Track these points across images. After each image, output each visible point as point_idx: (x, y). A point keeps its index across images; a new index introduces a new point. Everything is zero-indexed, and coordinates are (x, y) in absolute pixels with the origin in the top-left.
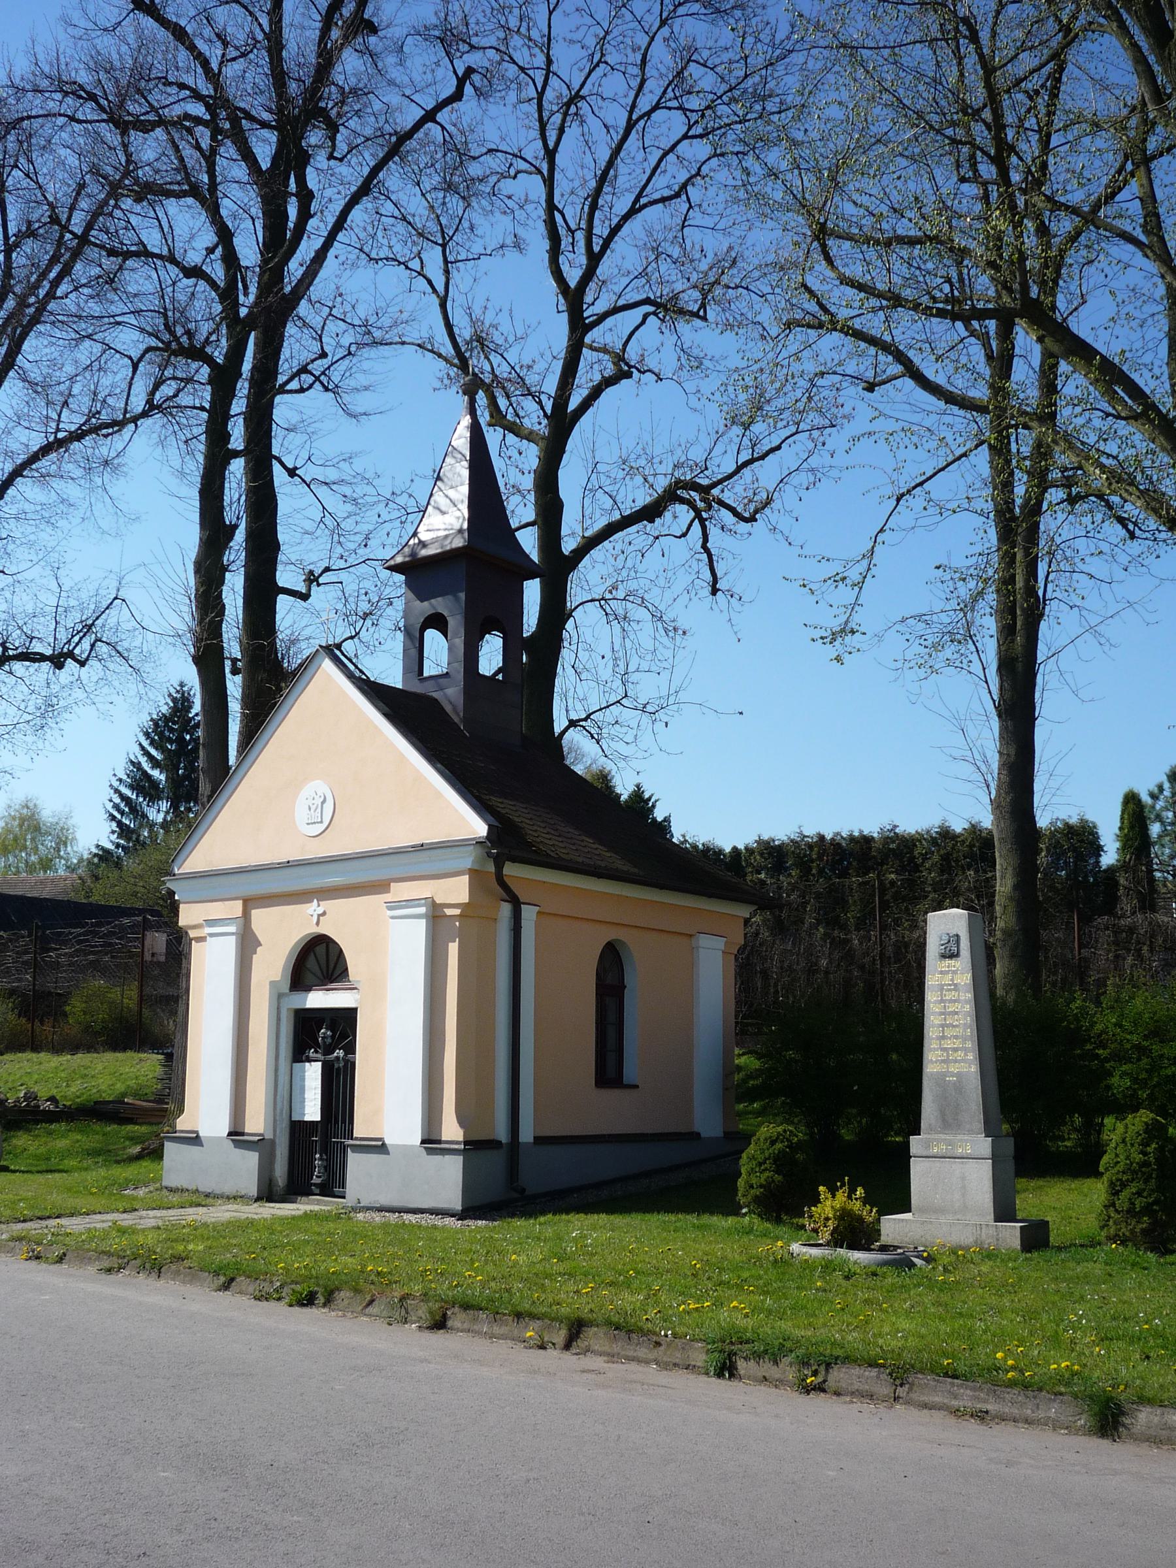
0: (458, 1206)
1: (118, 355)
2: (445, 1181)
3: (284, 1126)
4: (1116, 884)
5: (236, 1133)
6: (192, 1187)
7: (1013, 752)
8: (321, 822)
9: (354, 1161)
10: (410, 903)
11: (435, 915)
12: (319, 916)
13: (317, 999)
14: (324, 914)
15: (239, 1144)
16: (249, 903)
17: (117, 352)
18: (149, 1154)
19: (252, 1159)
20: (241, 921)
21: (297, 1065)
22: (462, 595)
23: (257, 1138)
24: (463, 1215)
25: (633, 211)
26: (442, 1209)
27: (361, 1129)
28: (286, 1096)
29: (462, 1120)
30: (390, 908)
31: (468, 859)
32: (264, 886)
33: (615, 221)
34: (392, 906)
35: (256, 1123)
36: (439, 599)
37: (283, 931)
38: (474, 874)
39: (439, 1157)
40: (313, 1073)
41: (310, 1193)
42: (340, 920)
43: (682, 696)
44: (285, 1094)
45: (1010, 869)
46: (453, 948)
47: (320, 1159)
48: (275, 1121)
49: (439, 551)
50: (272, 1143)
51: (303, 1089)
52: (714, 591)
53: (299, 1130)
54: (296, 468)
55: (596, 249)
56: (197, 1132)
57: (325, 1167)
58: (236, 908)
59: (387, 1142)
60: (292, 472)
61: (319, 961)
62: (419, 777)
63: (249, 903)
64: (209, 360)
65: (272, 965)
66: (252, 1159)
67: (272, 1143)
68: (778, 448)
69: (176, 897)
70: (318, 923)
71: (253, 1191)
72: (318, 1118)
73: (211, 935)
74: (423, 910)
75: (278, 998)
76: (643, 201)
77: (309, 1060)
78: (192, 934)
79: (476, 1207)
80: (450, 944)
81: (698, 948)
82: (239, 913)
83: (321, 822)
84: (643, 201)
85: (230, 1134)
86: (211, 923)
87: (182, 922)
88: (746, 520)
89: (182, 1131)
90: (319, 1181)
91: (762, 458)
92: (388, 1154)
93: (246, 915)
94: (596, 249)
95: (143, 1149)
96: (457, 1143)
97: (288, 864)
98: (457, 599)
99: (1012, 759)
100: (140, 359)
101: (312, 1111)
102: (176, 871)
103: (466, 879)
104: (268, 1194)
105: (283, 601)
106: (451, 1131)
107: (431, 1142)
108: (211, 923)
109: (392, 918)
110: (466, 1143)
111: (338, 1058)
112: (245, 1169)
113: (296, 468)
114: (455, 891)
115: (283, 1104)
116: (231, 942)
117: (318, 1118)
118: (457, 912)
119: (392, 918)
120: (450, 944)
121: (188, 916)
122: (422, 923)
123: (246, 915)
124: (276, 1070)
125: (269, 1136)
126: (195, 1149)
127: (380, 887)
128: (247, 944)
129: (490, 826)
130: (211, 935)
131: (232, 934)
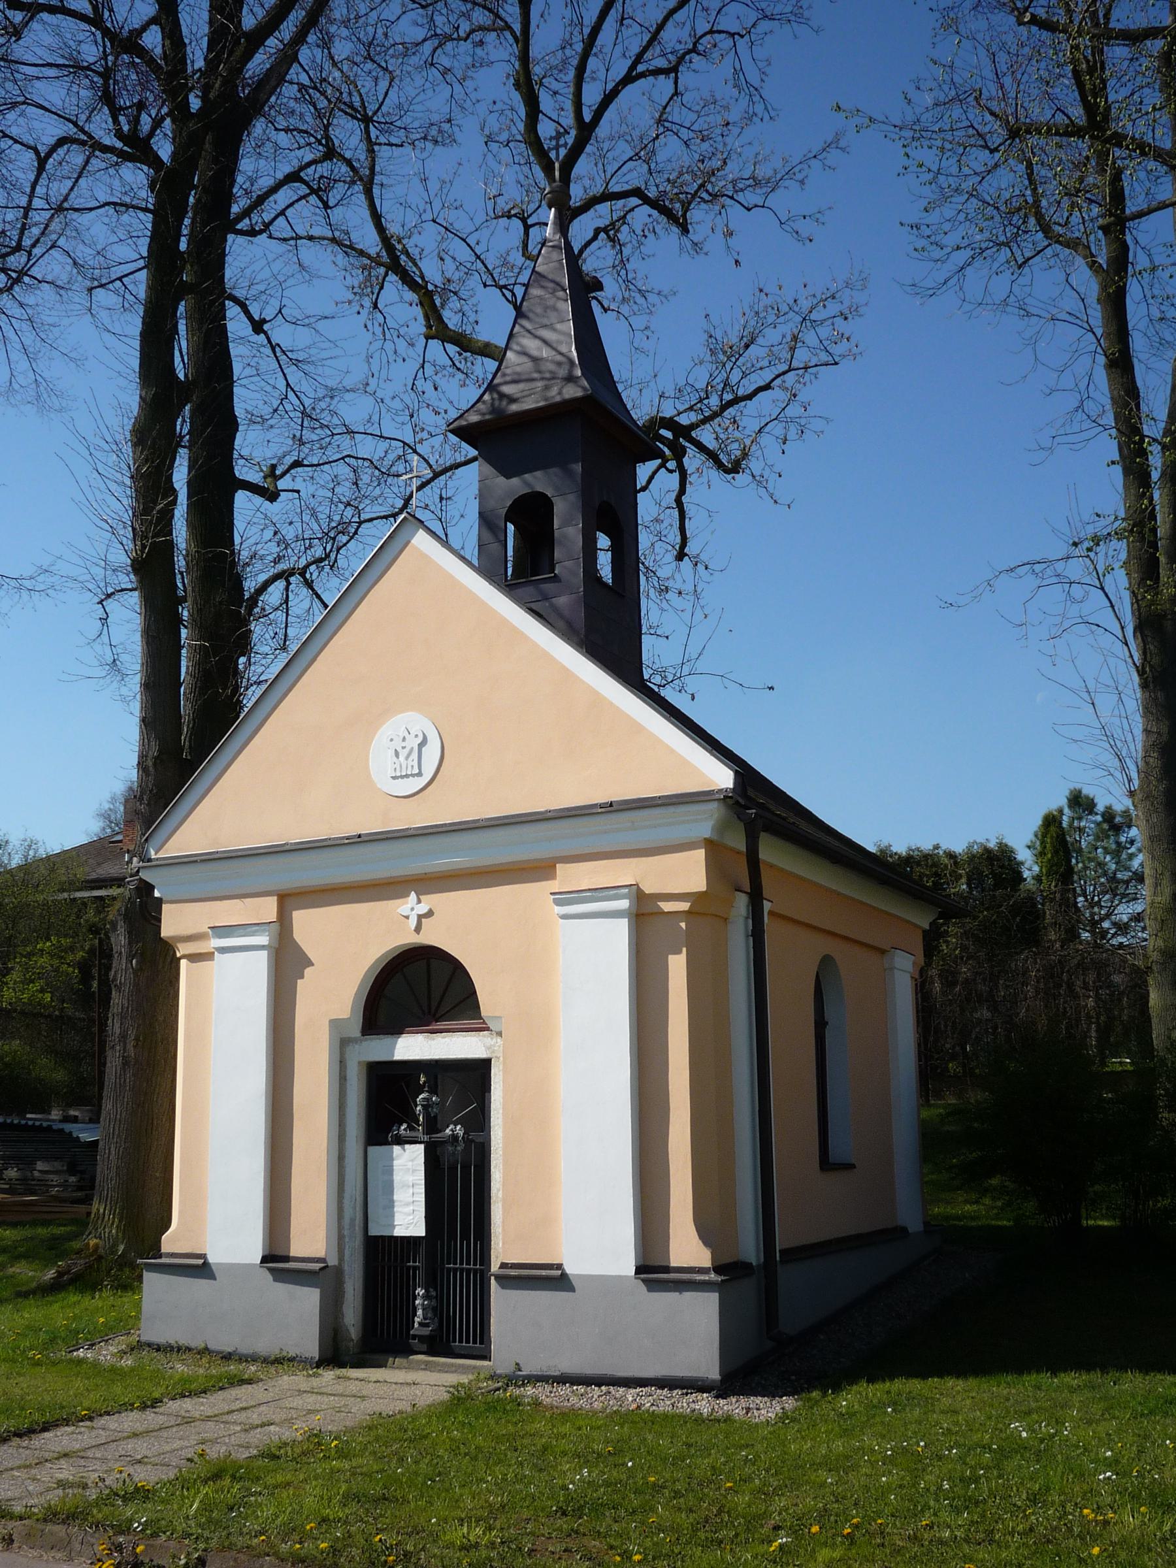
0: (713, 1373)
1: (17, 147)
2: (691, 1334)
3: (355, 1246)
4: (1039, 916)
5: (275, 1258)
6: (197, 1343)
7: (1165, 729)
8: (420, 774)
9: (503, 1304)
10: (598, 893)
11: (644, 912)
12: (420, 917)
13: (413, 1047)
14: (430, 914)
15: (281, 1276)
16: (288, 901)
17: (16, 141)
18: (72, 1281)
19: (309, 1299)
20: (276, 927)
21: (373, 1150)
22: (578, 468)
23: (317, 1266)
24: (725, 1388)
25: (629, 79)
26: (697, 1380)
27: (507, 1244)
28: (360, 1199)
29: (706, 1232)
30: (558, 903)
31: (705, 821)
32: (305, 877)
33: (610, 86)
34: (562, 898)
35: (311, 1238)
36: (538, 474)
37: (348, 945)
38: (712, 847)
39: (674, 1296)
40: (408, 1165)
41: (407, 1351)
42: (453, 923)
43: (700, 666)
44: (360, 1195)
45: (1168, 874)
46: (677, 965)
47: (425, 1297)
48: (341, 1237)
49: (542, 404)
50: (338, 1272)
51: (389, 1188)
52: (681, 556)
53: (384, 1255)
54: (264, 321)
55: (587, 117)
56: (203, 1256)
57: (434, 1309)
58: (268, 908)
59: (569, 1270)
60: (258, 326)
61: (421, 986)
62: (597, 700)
63: (288, 901)
64: (153, 161)
65: (333, 992)
66: (309, 1299)
67: (338, 1272)
68: (767, 387)
69: (157, 894)
70: (418, 929)
71: (312, 1348)
72: (420, 1231)
73: (223, 950)
74: (624, 904)
75: (342, 1044)
76: (641, 68)
77: (401, 1141)
78: (182, 950)
79: (737, 1378)
80: (672, 959)
81: (892, 969)
82: (272, 915)
83: (420, 774)
84: (641, 68)
85: (265, 1260)
86: (221, 931)
87: (166, 931)
88: (727, 471)
89: (173, 1255)
90: (426, 1331)
91: (749, 397)
92: (215, 1279)
93: (284, 921)
94: (587, 117)
95: (60, 1274)
96: (701, 1271)
97: (359, 840)
98: (570, 474)
99: (1165, 738)
100: (49, 154)
101: (408, 1217)
102: (153, 855)
103: (700, 854)
104: (335, 1354)
105: (241, 497)
106: (687, 1249)
107: (653, 1270)
108: (221, 931)
109: (565, 917)
110: (717, 1269)
111: (455, 1137)
112: (297, 1317)
113: (264, 321)
114: (684, 874)
115: (352, 1210)
116: (261, 961)
117: (420, 1231)
118: (684, 906)
119: (565, 917)
120: (672, 959)
121: (174, 922)
122: (623, 925)
123: (284, 921)
124: (341, 1158)
125: (333, 1261)
126: (202, 1283)
127: (541, 870)
128: (287, 964)
129: (736, 773)
130: (223, 950)
131: (262, 947)
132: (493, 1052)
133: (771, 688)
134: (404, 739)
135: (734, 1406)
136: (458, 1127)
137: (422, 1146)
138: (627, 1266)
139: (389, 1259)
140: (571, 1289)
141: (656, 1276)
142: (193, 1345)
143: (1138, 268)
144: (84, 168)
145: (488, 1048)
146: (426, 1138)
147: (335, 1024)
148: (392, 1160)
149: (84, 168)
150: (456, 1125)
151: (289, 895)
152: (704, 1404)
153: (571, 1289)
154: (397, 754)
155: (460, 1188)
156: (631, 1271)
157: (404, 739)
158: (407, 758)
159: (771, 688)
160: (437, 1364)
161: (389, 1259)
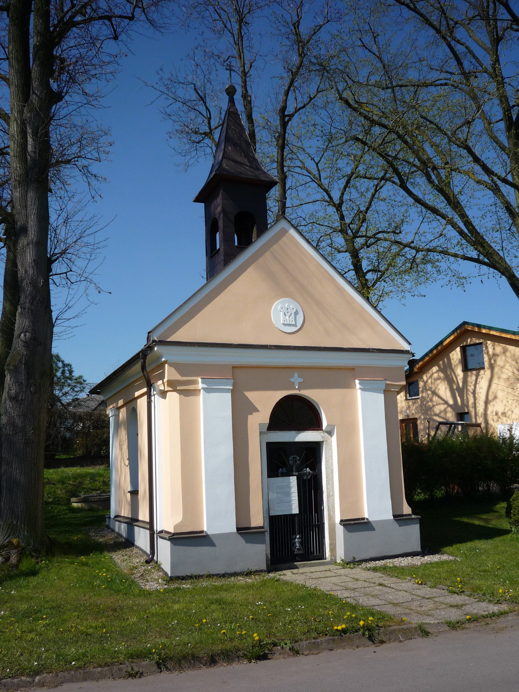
0: (418, 548)
2: (412, 534)
5: (244, 530)
6: (206, 573)
24: (423, 554)
90: (301, 552)
106: (407, 510)
112: (259, 553)
132: (325, 439)
133: (110, 293)
134: (288, 309)
135: (427, 559)
136: (308, 469)
137: (296, 477)
138: (390, 516)
139: (279, 525)
140: (213, 544)
141: (249, 531)
142: (202, 573)
143: (327, 207)
144: (460, 127)
145: (323, 437)
146: (297, 474)
147: (260, 425)
148: (290, 483)
149: (460, 127)
150: (306, 468)
151: (236, 367)
152: (417, 561)
153: (213, 544)
154: (285, 314)
155: (311, 492)
156: (235, 530)
157: (288, 309)
158: (289, 317)
159: (110, 293)
160: (309, 564)
161: (279, 525)
